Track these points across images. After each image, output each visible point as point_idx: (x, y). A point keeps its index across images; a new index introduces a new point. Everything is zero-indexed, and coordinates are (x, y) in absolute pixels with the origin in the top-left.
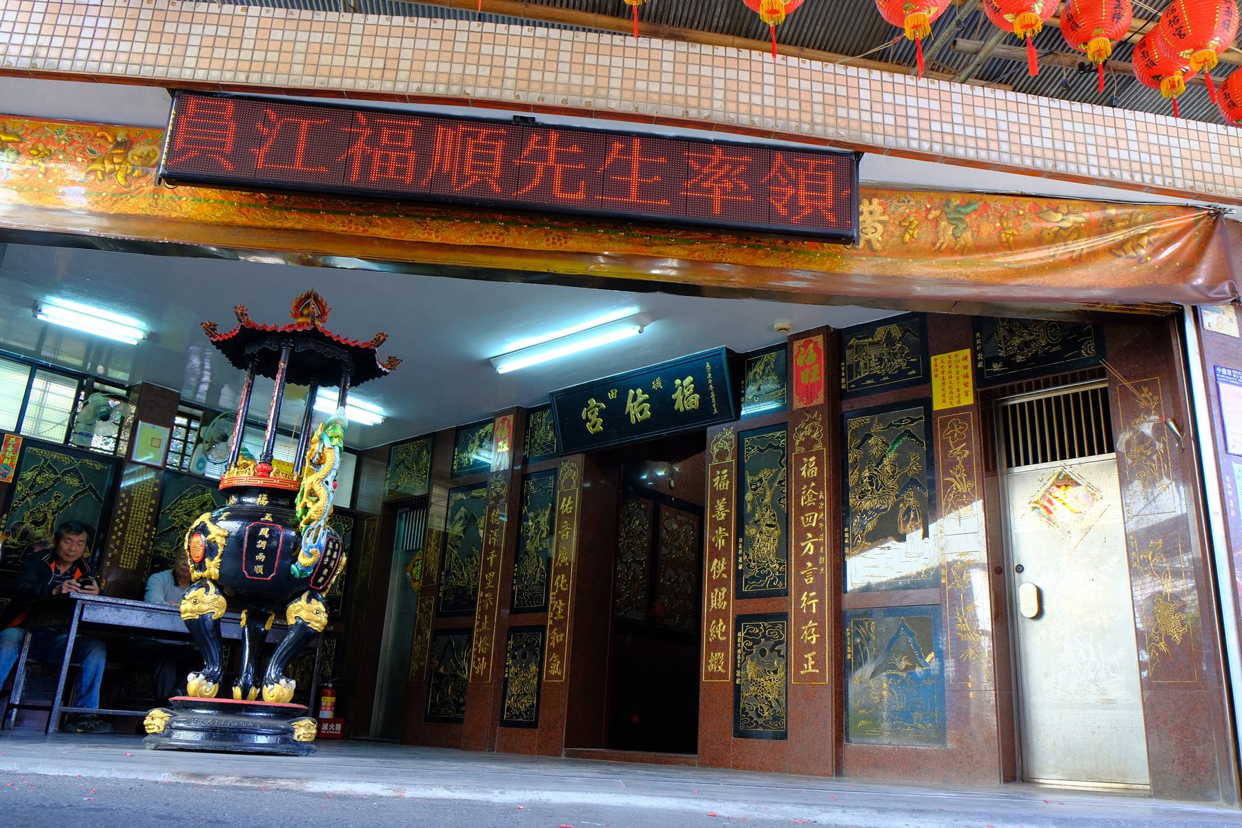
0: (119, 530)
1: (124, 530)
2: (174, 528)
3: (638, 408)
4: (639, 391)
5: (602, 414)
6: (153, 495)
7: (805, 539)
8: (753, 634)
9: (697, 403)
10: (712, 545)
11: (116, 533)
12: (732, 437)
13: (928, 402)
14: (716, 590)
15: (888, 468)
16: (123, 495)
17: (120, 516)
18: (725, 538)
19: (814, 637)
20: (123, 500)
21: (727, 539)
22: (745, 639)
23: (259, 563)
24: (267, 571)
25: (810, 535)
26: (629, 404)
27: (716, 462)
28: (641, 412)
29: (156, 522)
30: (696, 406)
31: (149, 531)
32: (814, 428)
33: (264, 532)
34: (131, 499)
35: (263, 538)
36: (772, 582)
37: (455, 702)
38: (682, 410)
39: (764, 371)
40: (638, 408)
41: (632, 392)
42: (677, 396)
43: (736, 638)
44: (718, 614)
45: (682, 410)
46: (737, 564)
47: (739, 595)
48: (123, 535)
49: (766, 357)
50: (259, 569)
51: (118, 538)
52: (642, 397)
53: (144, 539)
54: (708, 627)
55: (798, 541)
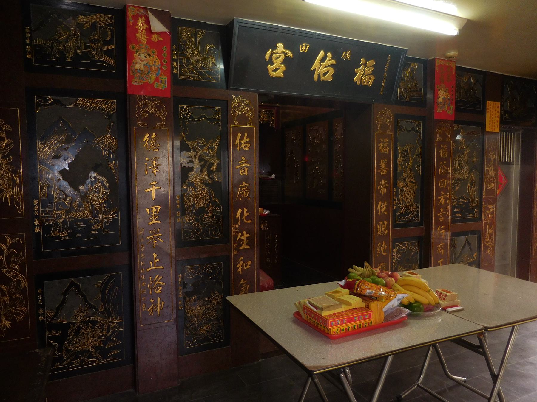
5: (286, 61)
7: (440, 195)
8: (402, 250)
10: (378, 191)
12: (392, 116)
13: (483, 126)
14: (381, 223)
15: (466, 157)
18: (386, 187)
19: (442, 251)
21: (388, 188)
22: (397, 253)
25: (442, 193)
27: (380, 132)
36: (412, 217)
37: (79, 328)
40: (323, 67)
41: (322, 54)
42: (360, 72)
43: (392, 252)
44: (384, 237)
46: (393, 205)
47: (395, 226)
49: (412, 65)
52: (330, 61)
54: (376, 248)
55: (437, 196)
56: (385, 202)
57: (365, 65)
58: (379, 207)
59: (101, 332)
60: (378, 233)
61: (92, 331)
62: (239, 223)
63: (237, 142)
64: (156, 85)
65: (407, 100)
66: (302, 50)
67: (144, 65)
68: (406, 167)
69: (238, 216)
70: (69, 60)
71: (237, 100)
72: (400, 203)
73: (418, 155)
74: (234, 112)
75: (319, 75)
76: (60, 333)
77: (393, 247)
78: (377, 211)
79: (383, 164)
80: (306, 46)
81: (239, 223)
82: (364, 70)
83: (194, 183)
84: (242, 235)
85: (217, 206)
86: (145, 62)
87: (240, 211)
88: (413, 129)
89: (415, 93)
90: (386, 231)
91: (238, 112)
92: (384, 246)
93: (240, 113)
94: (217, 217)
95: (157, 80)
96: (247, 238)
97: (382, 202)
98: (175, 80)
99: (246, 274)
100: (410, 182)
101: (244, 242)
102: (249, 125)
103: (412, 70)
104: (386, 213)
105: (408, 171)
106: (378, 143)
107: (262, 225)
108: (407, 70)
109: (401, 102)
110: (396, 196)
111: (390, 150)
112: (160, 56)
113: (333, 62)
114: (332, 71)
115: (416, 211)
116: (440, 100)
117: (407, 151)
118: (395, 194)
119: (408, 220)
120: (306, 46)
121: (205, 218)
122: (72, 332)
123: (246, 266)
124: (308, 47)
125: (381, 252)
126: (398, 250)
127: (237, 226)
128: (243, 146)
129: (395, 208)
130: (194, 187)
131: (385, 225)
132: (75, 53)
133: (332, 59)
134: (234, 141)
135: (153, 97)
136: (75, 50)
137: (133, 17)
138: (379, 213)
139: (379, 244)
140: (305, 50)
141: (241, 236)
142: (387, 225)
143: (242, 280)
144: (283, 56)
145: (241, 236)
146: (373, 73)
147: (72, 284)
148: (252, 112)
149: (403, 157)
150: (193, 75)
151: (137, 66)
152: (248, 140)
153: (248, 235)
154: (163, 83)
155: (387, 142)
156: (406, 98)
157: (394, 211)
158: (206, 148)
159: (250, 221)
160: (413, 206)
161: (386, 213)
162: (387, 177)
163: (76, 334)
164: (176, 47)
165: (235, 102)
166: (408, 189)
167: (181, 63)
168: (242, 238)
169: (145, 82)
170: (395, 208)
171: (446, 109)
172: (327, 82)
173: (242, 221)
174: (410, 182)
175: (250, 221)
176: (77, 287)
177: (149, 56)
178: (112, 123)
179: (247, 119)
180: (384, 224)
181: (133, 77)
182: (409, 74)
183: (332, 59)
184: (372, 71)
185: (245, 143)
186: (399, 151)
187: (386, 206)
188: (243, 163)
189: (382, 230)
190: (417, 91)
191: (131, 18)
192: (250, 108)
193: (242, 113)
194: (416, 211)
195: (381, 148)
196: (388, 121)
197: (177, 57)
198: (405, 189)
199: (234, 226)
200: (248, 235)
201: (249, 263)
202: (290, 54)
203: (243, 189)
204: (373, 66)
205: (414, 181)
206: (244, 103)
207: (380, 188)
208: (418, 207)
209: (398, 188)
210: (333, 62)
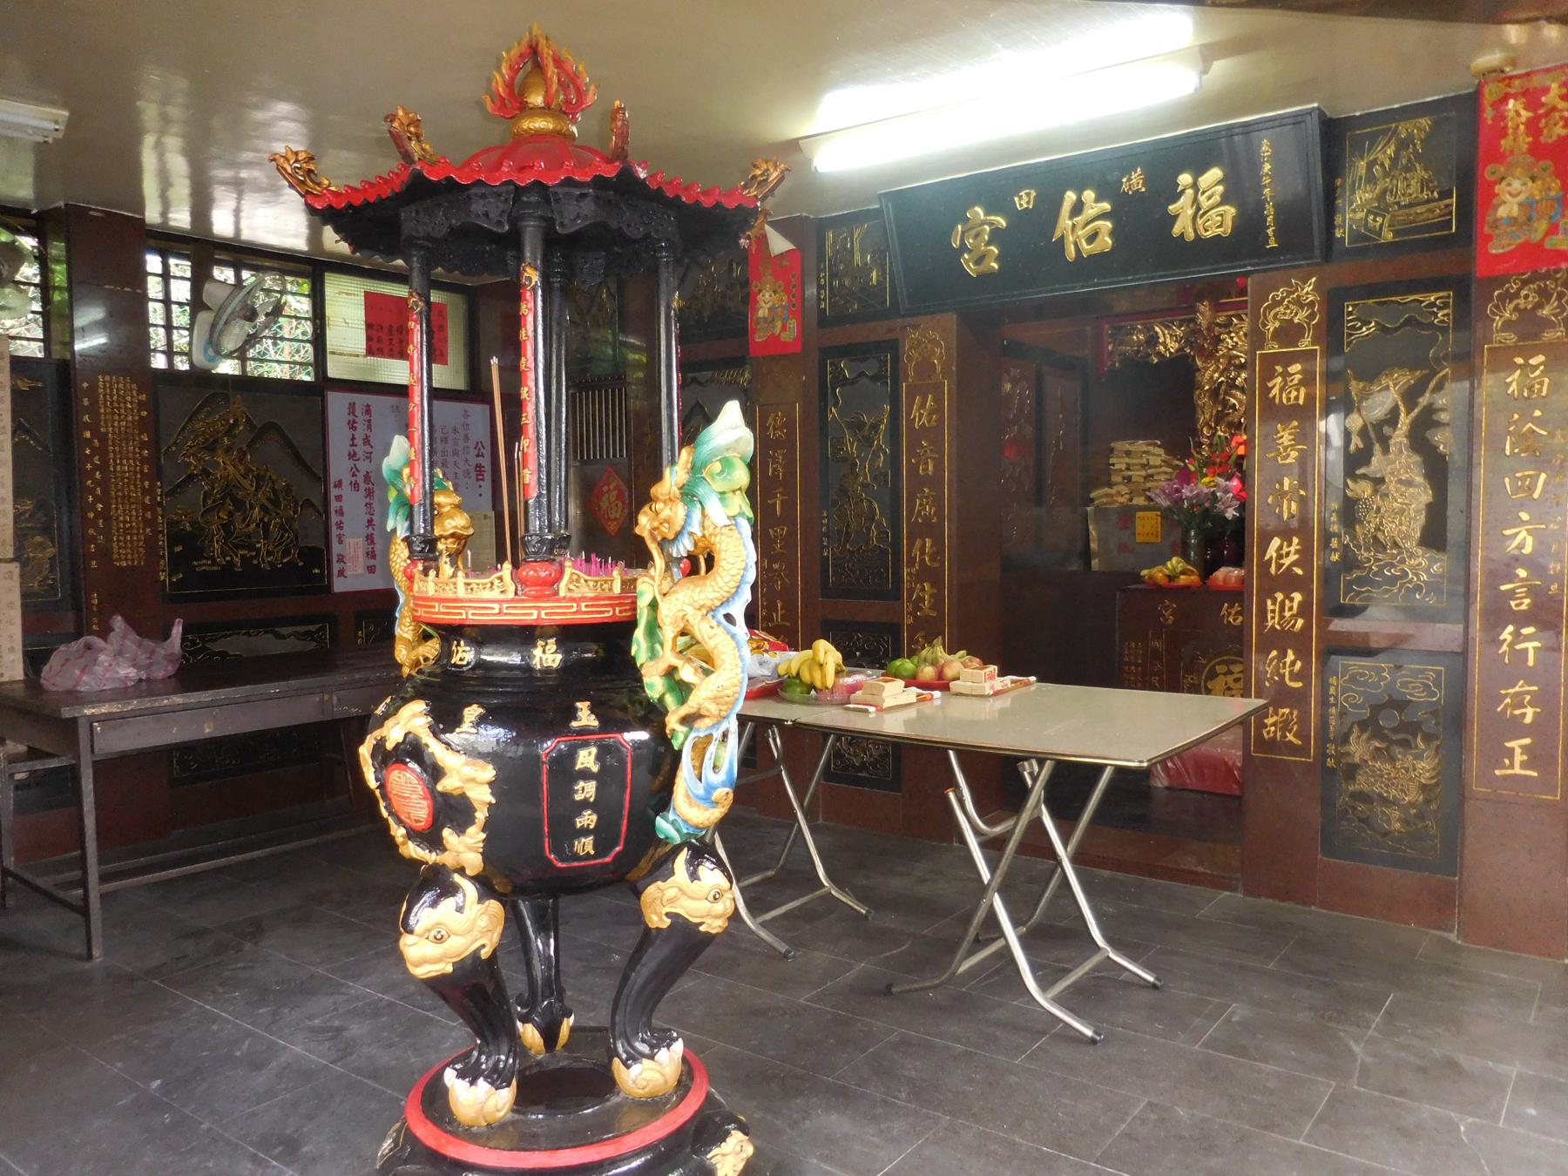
0: (97, 499)
1: (105, 498)
2: (190, 477)
3: (1085, 227)
4: (1089, 195)
6: (142, 425)
8: (1365, 684)
9: (1229, 223)
11: (93, 507)
14: (1280, 596)
16: (88, 435)
17: (91, 475)
20: (89, 442)
23: (585, 832)
24: (601, 847)
25: (1525, 516)
26: (1065, 222)
28: (1092, 238)
29: (157, 473)
30: (1226, 230)
31: (150, 492)
32: (1545, 295)
33: (587, 759)
34: (103, 438)
35: (586, 775)
38: (1190, 236)
39: (1394, 160)
41: (1070, 196)
42: (1182, 207)
45: (1190, 236)
48: (106, 491)
50: (586, 845)
51: (97, 499)
52: (1094, 205)
53: (145, 508)
56: (1295, 540)
57: (1195, 186)
60: (1270, 624)
67: (1520, 205)
80: (1028, 195)
86: (1522, 198)
90: (1300, 622)
92: (1293, 663)
95: (784, 328)
102: (1305, 344)
114: (1107, 225)
115: (1427, 571)
116: (763, 312)
124: (1033, 194)
131: (1295, 605)
133: (1097, 200)
138: (1273, 569)
139: (1274, 653)
146: (1225, 199)
151: (761, 313)
171: (777, 331)
177: (1533, 179)
180: (1292, 600)
183: (1097, 200)
187: (1297, 552)
195: (1275, 391)
202: (1002, 222)
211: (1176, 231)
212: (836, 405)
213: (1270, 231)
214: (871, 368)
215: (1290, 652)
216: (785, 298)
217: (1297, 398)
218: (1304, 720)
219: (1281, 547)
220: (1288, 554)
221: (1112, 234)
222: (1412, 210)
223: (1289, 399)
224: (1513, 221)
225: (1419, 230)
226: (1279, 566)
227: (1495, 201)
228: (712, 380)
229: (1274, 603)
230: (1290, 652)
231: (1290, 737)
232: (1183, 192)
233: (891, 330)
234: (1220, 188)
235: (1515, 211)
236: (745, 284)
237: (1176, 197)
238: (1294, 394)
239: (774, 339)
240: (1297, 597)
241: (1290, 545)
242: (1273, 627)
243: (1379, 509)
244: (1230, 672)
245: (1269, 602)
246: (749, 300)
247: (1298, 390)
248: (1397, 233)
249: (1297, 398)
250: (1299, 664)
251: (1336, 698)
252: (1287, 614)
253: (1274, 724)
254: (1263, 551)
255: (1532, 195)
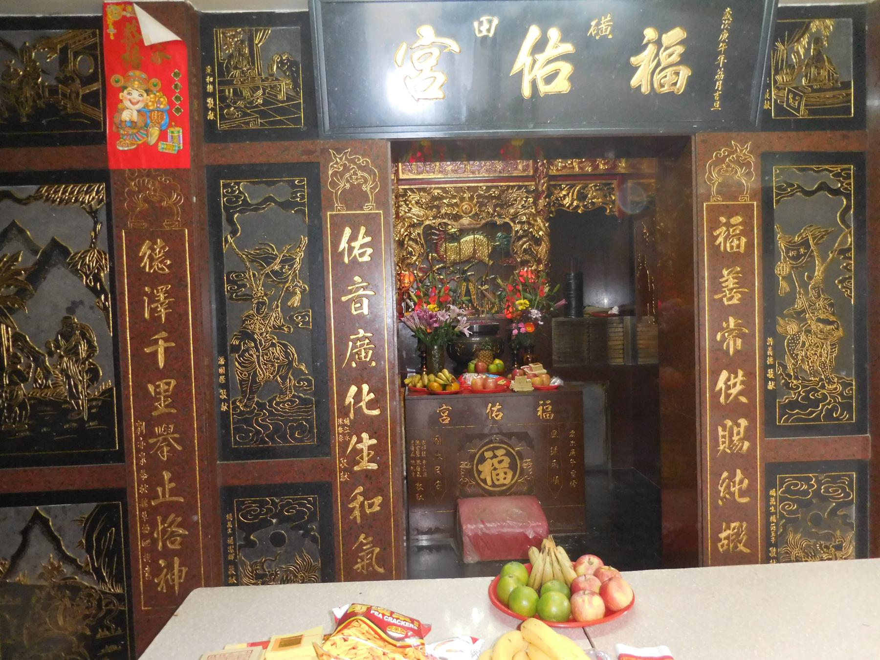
4: (554, 34)
8: (798, 492)
12: (752, 159)
14: (729, 423)
18: (742, 336)
21: (748, 339)
22: (782, 499)
26: (523, 59)
27: (717, 200)
28: (549, 79)
37: (50, 597)
38: (646, 89)
41: (534, 33)
42: (644, 61)
46: (766, 380)
49: (815, 25)
54: (715, 483)
56: (740, 373)
57: (658, 43)
58: (721, 384)
59: (87, 608)
60: (721, 447)
61: (72, 605)
62: (352, 416)
63: (343, 245)
64: (162, 147)
65: (802, 113)
66: (480, 31)
67: (139, 111)
68: (804, 285)
69: (350, 399)
70: (25, 120)
71: (341, 159)
72: (790, 376)
73: (844, 252)
74: (334, 184)
75: (534, 84)
76: (18, 601)
77: (769, 484)
78: (716, 395)
79: (729, 278)
80: (490, 22)
81: (352, 416)
82: (657, 55)
83: (254, 333)
84: (360, 440)
85: (303, 380)
86: (140, 106)
87: (353, 389)
88: (823, 187)
89: (829, 95)
90: (746, 445)
91: (343, 185)
92: (741, 482)
93: (348, 186)
94: (304, 402)
95: (163, 136)
96: (370, 447)
97: (730, 373)
98: (208, 133)
99: (374, 525)
100: (819, 320)
101: (365, 453)
102: (369, 208)
103: (817, 39)
104: (743, 399)
105: (812, 293)
106: (712, 229)
107: (540, 409)
108: (798, 41)
109: (781, 121)
110: (775, 357)
111: (750, 245)
112: (167, 90)
113: (568, 48)
114: (566, 69)
115: (841, 394)
117: (806, 244)
118: (770, 353)
119: (817, 419)
120: (490, 22)
121: (278, 404)
122: (37, 601)
123: (371, 506)
125: (732, 494)
126: (788, 490)
127: (347, 422)
128: (356, 252)
129: (771, 386)
130: (255, 341)
131: (742, 430)
132: (35, 107)
133: (563, 40)
134: (336, 243)
135: (156, 171)
136: (34, 101)
137: (116, 24)
140: (489, 30)
141: (357, 443)
142: (747, 429)
143: (363, 536)
144: (436, 52)
145: (357, 443)
146: (684, 60)
147: (37, 516)
148: (374, 181)
149: (793, 258)
150: (247, 119)
151: (126, 116)
152: (368, 239)
153: (374, 441)
154: (175, 142)
155: (740, 224)
156: (798, 110)
157: (770, 398)
158: (278, 260)
159: (376, 412)
160: (830, 382)
161: (743, 399)
162: (743, 311)
163: (46, 607)
164: (213, 70)
165: (337, 163)
166: (813, 339)
167: (223, 99)
168: (359, 446)
169: (140, 142)
170: (771, 386)
172: (559, 96)
173: (359, 411)
174: (819, 320)
175: (376, 412)
176: (45, 522)
177: (148, 91)
178: (99, 227)
179: (365, 197)
180: (738, 425)
181: (117, 136)
182: (807, 50)
183: (563, 40)
184: (681, 55)
185: (362, 246)
186: (782, 245)
187: (742, 383)
188: (358, 289)
189: (731, 441)
190: (833, 89)
191: (111, 27)
192: (370, 172)
193: (352, 185)
194: (841, 394)
195: (721, 239)
196: (741, 172)
197: (214, 88)
198: (803, 338)
199: (340, 421)
200: (374, 441)
201: (378, 500)
203: (359, 343)
204: (682, 43)
205: (832, 318)
206: (355, 164)
207: (724, 339)
208: (846, 385)
209: (779, 339)
210: (568, 48)
211: (634, 82)
212: (234, 233)
213: (717, 95)
214: (280, 191)
215: (739, 472)
216: (164, 100)
217: (738, 246)
218: (751, 533)
219: (728, 379)
220: (735, 385)
221: (571, 79)
222: (822, 95)
223: (732, 247)
224: (133, 124)
225: (825, 111)
226: (728, 396)
227: (120, 106)
228: (37, 197)
229: (724, 430)
230: (739, 472)
231: (741, 547)
232: (647, 45)
233: (309, 152)
234: (680, 49)
235: (135, 117)
236: (99, 75)
237: (640, 48)
238: (736, 242)
239: (147, 150)
240: (743, 422)
241: (736, 377)
242: (724, 451)
243: (804, 343)
244: (495, 456)
245: (720, 429)
246: (103, 99)
247: (739, 239)
248: (811, 112)
249: (738, 246)
250: (746, 481)
251: (775, 506)
252: (735, 438)
253: (727, 538)
254: (714, 382)
255: (147, 105)
